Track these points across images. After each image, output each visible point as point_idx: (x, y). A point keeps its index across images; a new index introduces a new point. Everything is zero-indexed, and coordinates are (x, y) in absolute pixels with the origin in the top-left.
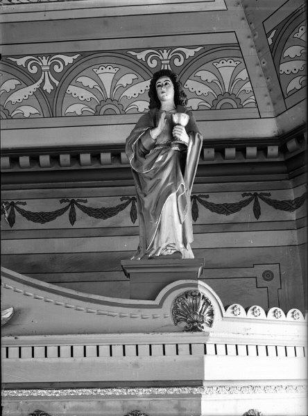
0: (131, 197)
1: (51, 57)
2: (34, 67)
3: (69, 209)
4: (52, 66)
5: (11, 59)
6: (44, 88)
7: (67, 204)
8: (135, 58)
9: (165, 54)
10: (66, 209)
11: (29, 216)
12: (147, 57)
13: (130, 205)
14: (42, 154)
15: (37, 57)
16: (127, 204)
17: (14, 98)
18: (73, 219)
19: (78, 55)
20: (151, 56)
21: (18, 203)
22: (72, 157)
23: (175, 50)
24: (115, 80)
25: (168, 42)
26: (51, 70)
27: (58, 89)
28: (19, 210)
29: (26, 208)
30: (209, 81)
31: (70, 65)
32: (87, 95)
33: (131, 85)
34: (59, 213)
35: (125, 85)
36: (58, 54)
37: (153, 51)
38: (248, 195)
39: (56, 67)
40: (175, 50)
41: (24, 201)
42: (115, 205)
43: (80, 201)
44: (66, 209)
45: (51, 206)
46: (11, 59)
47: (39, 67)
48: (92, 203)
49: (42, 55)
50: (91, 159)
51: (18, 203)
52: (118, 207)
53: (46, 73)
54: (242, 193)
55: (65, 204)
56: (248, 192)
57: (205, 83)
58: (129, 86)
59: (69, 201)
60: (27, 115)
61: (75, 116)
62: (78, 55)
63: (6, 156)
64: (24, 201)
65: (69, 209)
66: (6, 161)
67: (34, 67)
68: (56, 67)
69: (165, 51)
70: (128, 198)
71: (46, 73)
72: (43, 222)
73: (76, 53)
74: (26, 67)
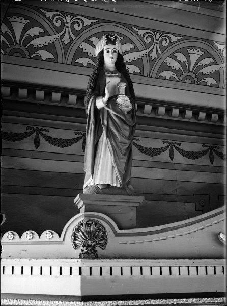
0: (35, 127)
1: (163, 34)
2: (59, 22)
3: (40, 136)
4: (72, 25)
5: (135, 28)
6: (151, 55)
7: (168, 144)
8: (136, 33)
9: (158, 36)
10: (167, 148)
11: (142, 149)
12: (144, 35)
13: (34, 134)
14: (187, 109)
15: (64, 14)
16: (32, 133)
17: (205, 71)
18: (172, 156)
19: (96, 21)
20: (149, 34)
21: (42, 129)
22: (46, 94)
23: (166, 34)
24: (199, 60)
25: (161, 26)
26: (160, 43)
27: (160, 57)
28: (215, 151)
29: (181, 147)
30: (182, 61)
31: (88, 26)
32: (177, 66)
33: (208, 65)
34: (163, 150)
35: (32, 36)
36: (169, 33)
37: (150, 31)
38: (31, 128)
39: (164, 42)
40: (166, 34)
41: (47, 128)
42: (158, 147)
43: (177, 144)
44: (167, 148)
45: (158, 144)
46: (135, 28)
47: (63, 23)
48: (54, 133)
49: (155, 31)
50: (193, 115)
51: (42, 129)
52: (161, 149)
53: (156, 44)
54: (76, 131)
55: (166, 145)
56: (31, 127)
57: (179, 62)
58: (206, 66)
59: (208, 146)
60: (208, 84)
61: (81, 65)
62: (96, 21)
63: (163, 106)
64: (47, 128)
65: (40, 136)
66: (6, 90)
67: (59, 22)
68: (164, 42)
69: (69, 16)
70: (81, 133)
71: (67, 29)
72: (62, 147)
73: (180, 35)
74: (144, 37)
